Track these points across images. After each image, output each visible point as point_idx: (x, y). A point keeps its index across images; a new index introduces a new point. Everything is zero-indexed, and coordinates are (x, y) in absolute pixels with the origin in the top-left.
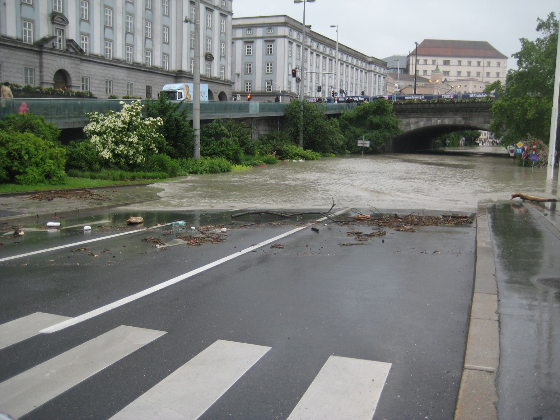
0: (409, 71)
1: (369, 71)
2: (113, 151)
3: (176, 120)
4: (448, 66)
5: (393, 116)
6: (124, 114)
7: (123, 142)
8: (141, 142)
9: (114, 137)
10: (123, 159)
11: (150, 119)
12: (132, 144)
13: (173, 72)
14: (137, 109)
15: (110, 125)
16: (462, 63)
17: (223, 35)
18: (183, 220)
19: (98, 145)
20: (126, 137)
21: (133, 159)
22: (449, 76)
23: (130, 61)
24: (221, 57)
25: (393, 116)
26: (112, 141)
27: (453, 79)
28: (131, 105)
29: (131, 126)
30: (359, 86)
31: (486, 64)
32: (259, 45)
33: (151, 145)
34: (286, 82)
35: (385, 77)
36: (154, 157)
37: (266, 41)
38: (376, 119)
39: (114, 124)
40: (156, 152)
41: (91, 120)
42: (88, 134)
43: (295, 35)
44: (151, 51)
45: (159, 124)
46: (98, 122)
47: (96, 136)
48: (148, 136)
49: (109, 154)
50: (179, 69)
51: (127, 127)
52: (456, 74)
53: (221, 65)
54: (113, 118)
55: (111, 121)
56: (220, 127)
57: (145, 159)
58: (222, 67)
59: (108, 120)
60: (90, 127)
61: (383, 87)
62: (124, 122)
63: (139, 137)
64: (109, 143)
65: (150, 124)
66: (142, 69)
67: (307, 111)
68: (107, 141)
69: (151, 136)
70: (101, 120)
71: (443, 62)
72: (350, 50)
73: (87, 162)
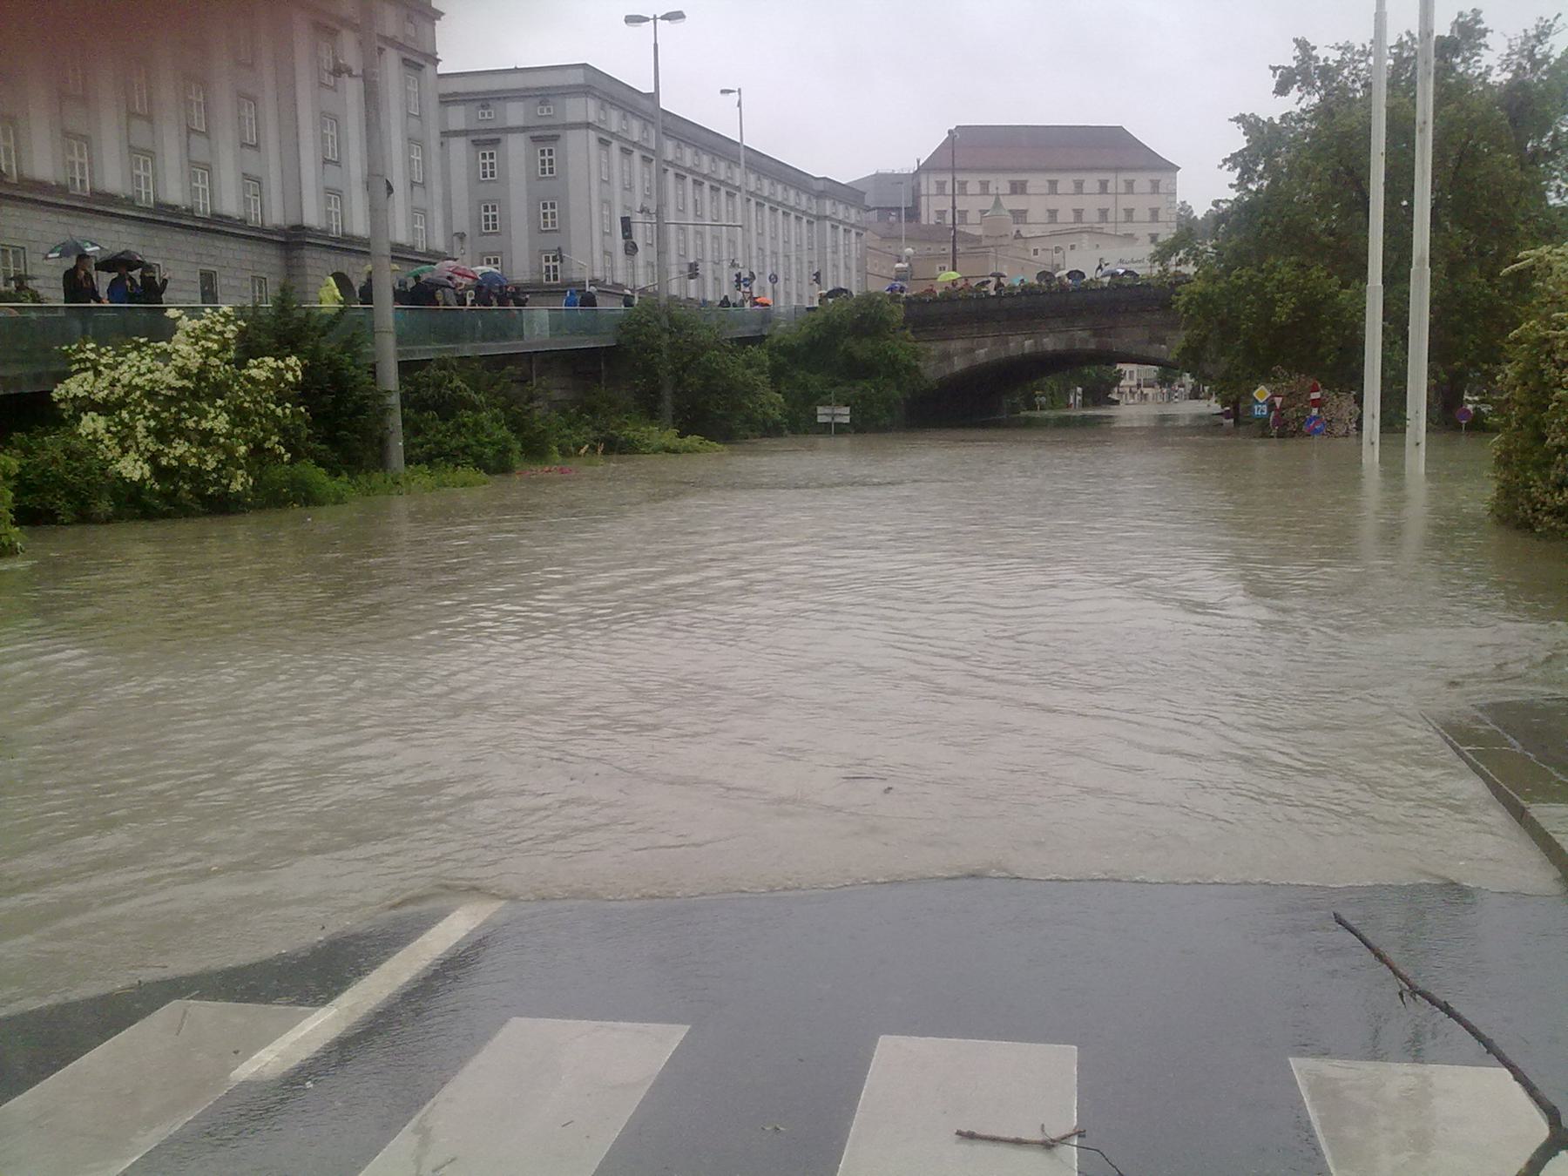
0: (920, 214)
1: (818, 218)
2: (153, 459)
3: (331, 362)
4: (1023, 198)
5: (905, 338)
6: (184, 348)
7: (183, 433)
8: (237, 431)
9: (154, 415)
10: (185, 483)
11: (263, 362)
12: (210, 437)
13: (278, 230)
14: (221, 333)
15: (138, 381)
17: (414, 122)
19: (102, 441)
20: (191, 417)
21: (217, 482)
22: (1026, 223)
23: (337, 232)
24: (413, 184)
25: (905, 338)
26: (148, 428)
27: (1037, 231)
28: (203, 321)
29: (203, 384)
30: (793, 259)
31: (1122, 188)
32: (516, 149)
33: (265, 439)
34: (597, 255)
35: (861, 231)
36: (277, 473)
37: (535, 139)
38: (862, 349)
39: (149, 376)
40: (285, 460)
41: (75, 367)
42: (66, 409)
43: (614, 121)
44: (208, 168)
45: (289, 376)
46: (98, 374)
47: (94, 414)
48: (259, 415)
49: (142, 468)
50: (293, 220)
51: (191, 386)
52: (1044, 217)
53: (415, 209)
54: (144, 361)
55: (139, 367)
56: (451, 382)
57: (251, 481)
58: (418, 213)
59: (130, 367)
60: (75, 387)
61: (858, 259)
62: (182, 373)
63: (233, 416)
64: (139, 436)
65: (268, 378)
66: (184, 222)
67: (680, 330)
68: (133, 428)
69: (266, 412)
70: (105, 366)
71: (1008, 185)
72: (764, 160)
73: (72, 493)
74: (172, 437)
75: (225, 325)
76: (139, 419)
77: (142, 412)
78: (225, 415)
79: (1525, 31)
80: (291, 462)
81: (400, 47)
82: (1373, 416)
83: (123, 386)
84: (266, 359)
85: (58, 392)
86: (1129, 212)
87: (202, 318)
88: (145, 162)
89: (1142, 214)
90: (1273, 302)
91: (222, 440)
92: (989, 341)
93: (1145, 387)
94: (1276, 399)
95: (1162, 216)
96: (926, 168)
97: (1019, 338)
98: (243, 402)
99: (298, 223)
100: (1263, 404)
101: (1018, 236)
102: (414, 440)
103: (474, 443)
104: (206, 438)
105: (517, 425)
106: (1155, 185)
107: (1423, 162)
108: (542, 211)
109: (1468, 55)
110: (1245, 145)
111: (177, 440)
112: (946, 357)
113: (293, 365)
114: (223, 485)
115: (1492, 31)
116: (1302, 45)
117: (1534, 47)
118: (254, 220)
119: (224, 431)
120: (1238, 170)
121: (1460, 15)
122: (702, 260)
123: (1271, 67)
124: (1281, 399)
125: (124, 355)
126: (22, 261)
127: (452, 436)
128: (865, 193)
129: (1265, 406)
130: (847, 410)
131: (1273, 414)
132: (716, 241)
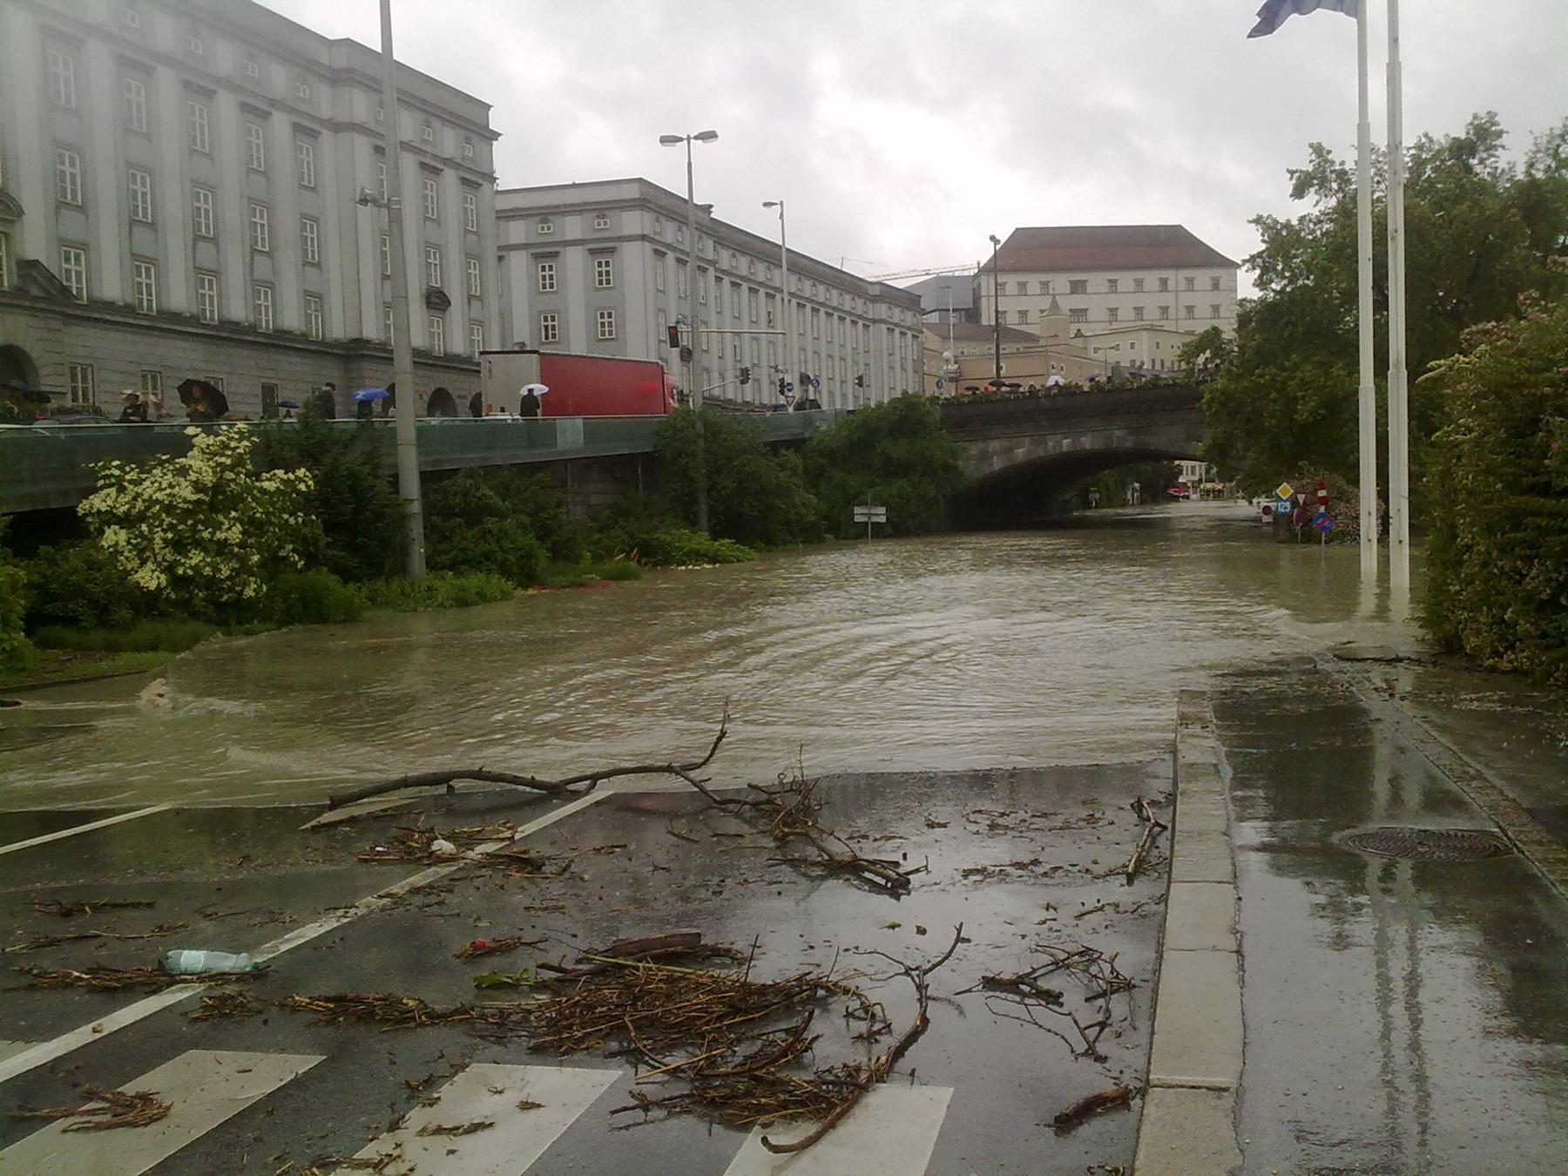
1: (874, 321)
2: (170, 569)
7: (200, 544)
9: (172, 527)
11: (275, 474)
13: (337, 344)
14: (234, 449)
15: (159, 495)
20: (207, 529)
26: (165, 540)
28: (220, 438)
31: (1182, 285)
32: (575, 262)
33: (281, 547)
37: (536, 256)
38: (898, 450)
39: (168, 491)
40: (299, 567)
41: (101, 482)
43: (669, 232)
44: (271, 286)
45: (302, 487)
47: (116, 527)
49: (158, 578)
51: (207, 499)
52: (1105, 315)
58: (475, 323)
59: (152, 483)
60: (98, 502)
62: (198, 486)
64: (157, 548)
68: (151, 540)
70: (130, 482)
72: (819, 267)
73: (94, 603)
74: (189, 547)
75: (240, 440)
76: (157, 532)
77: (160, 525)
78: (238, 525)
79: (1551, 129)
80: (307, 567)
81: (457, 166)
82: (1370, 514)
83: (144, 501)
84: (277, 471)
85: (83, 507)
87: (218, 435)
88: (210, 282)
90: (1295, 400)
91: (236, 550)
92: (1027, 441)
93: (1206, 481)
94: (1299, 496)
95: (1223, 312)
96: (984, 270)
97: (1059, 437)
98: (254, 513)
99: (357, 336)
100: (1285, 501)
101: (1079, 334)
102: (439, 547)
103: (497, 549)
104: (222, 548)
105: (544, 533)
107: (1396, 268)
108: (600, 320)
109: (1485, 155)
110: (1263, 247)
111: (193, 551)
112: (985, 456)
113: (302, 476)
114: (237, 592)
115: (1507, 132)
116: (1318, 149)
117: (1559, 146)
118: (316, 333)
119: (237, 540)
120: (1258, 272)
121: (1475, 117)
122: (757, 365)
123: (1288, 171)
124: (1304, 496)
125: (149, 472)
126: (90, 378)
127: (477, 544)
128: (920, 297)
129: (1288, 503)
130: (882, 510)
131: (1296, 511)
132: (771, 345)
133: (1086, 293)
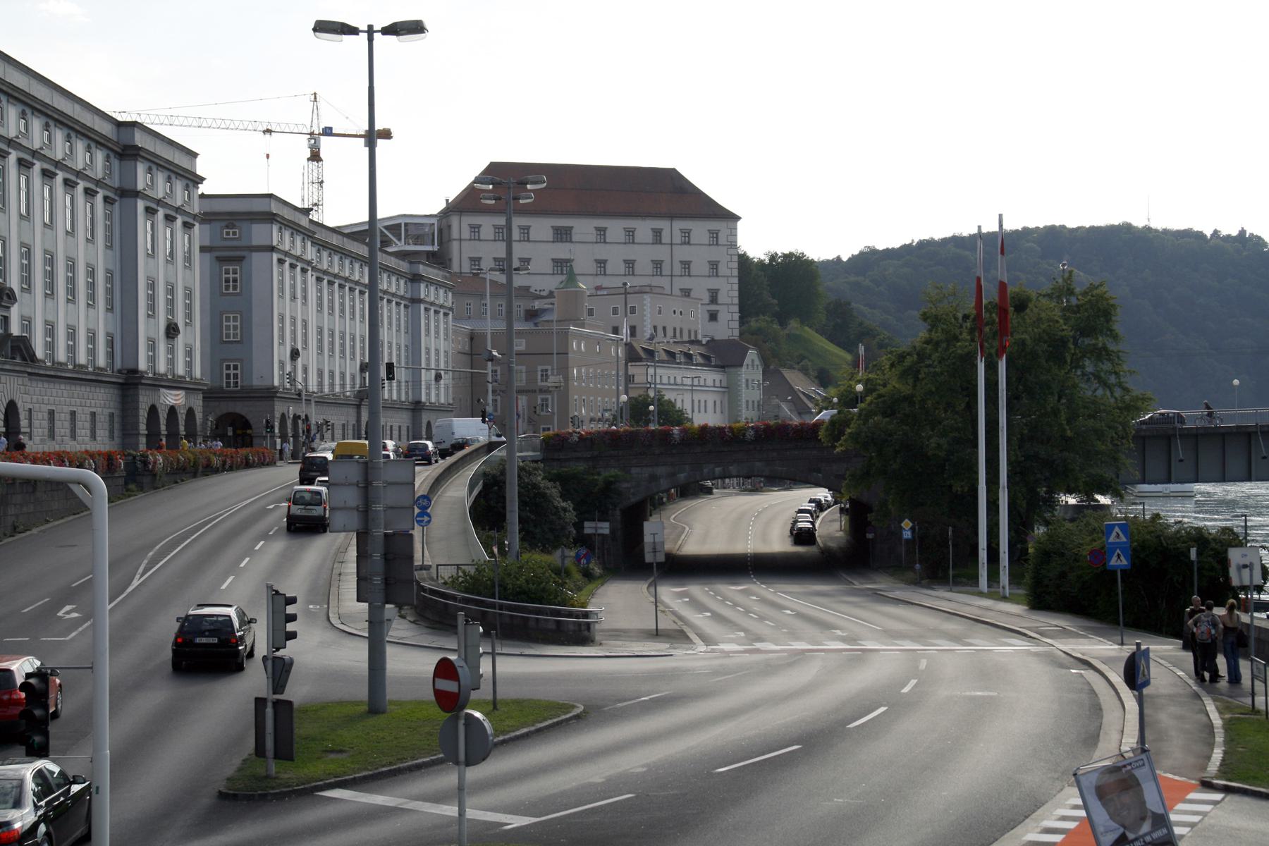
16: (532, 232)
18: (29, 829)
31: (678, 238)
86: (686, 265)
89: (700, 267)
95: (723, 269)
106: (714, 235)
133: (571, 241)
